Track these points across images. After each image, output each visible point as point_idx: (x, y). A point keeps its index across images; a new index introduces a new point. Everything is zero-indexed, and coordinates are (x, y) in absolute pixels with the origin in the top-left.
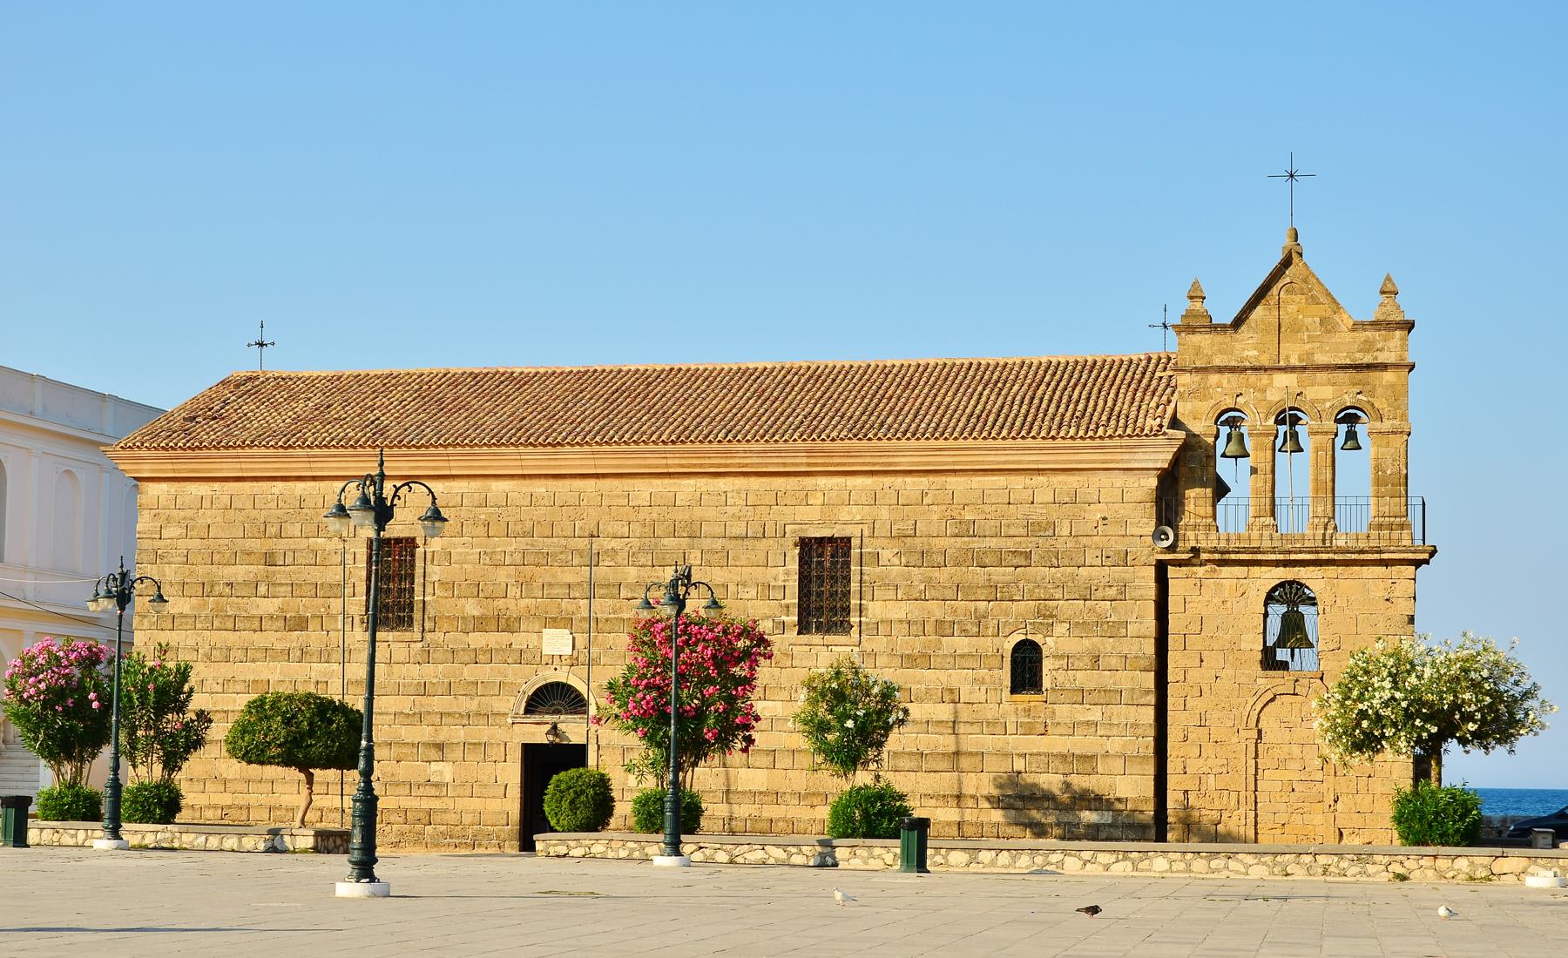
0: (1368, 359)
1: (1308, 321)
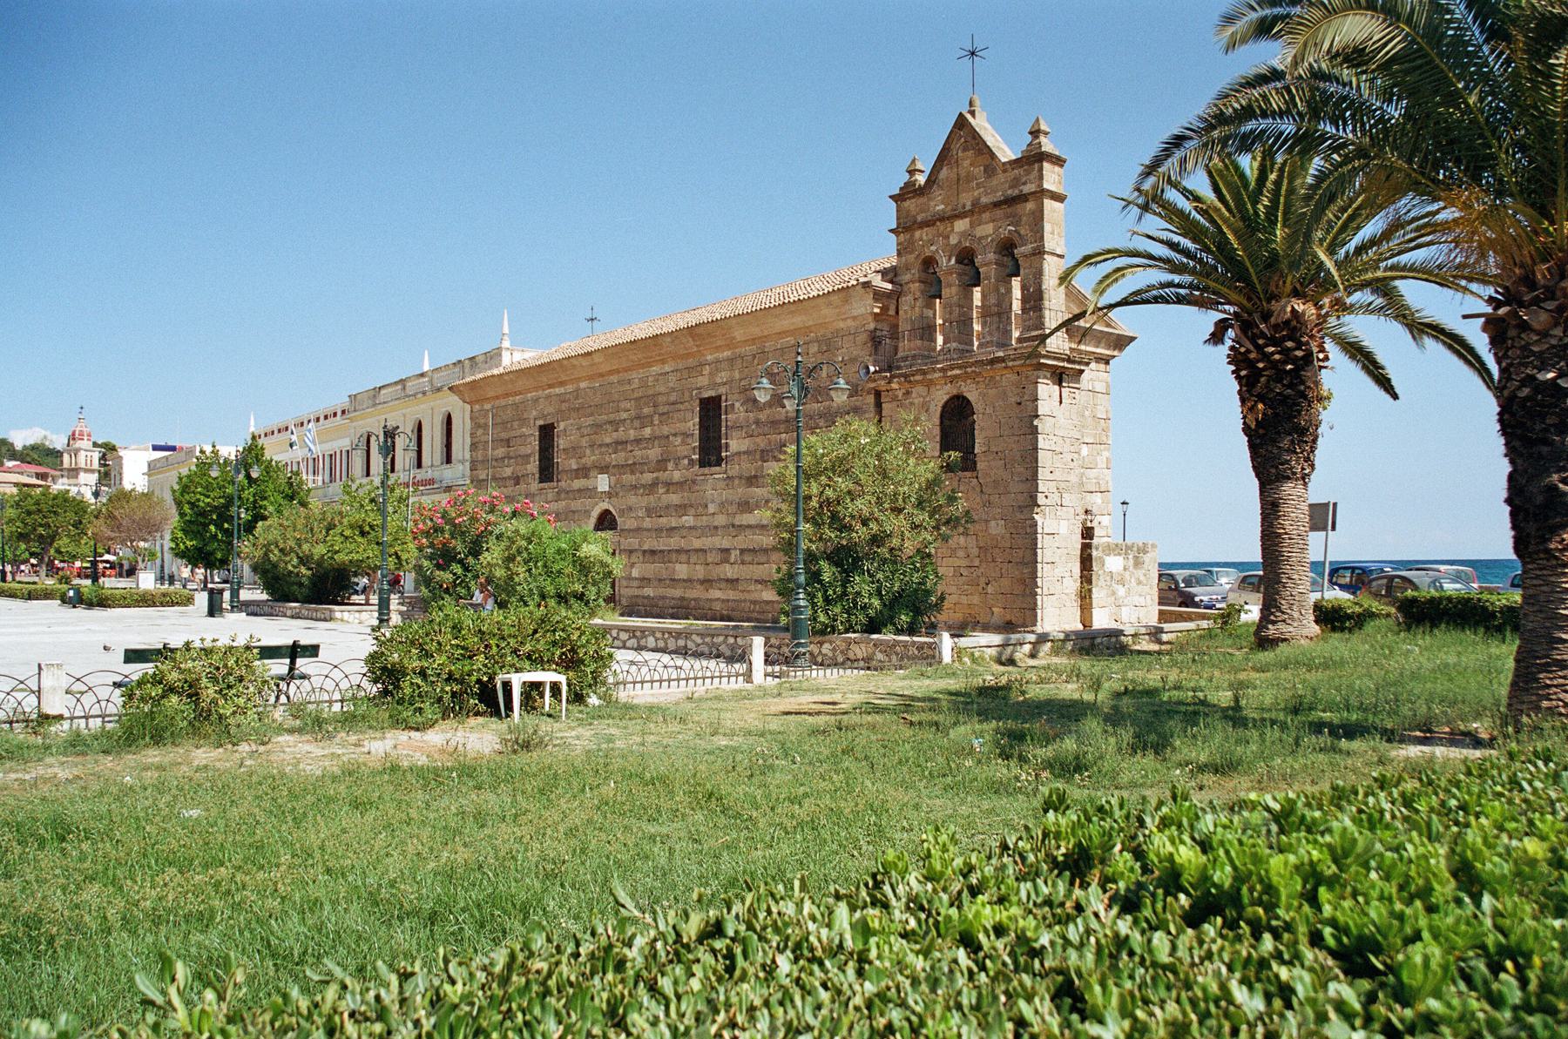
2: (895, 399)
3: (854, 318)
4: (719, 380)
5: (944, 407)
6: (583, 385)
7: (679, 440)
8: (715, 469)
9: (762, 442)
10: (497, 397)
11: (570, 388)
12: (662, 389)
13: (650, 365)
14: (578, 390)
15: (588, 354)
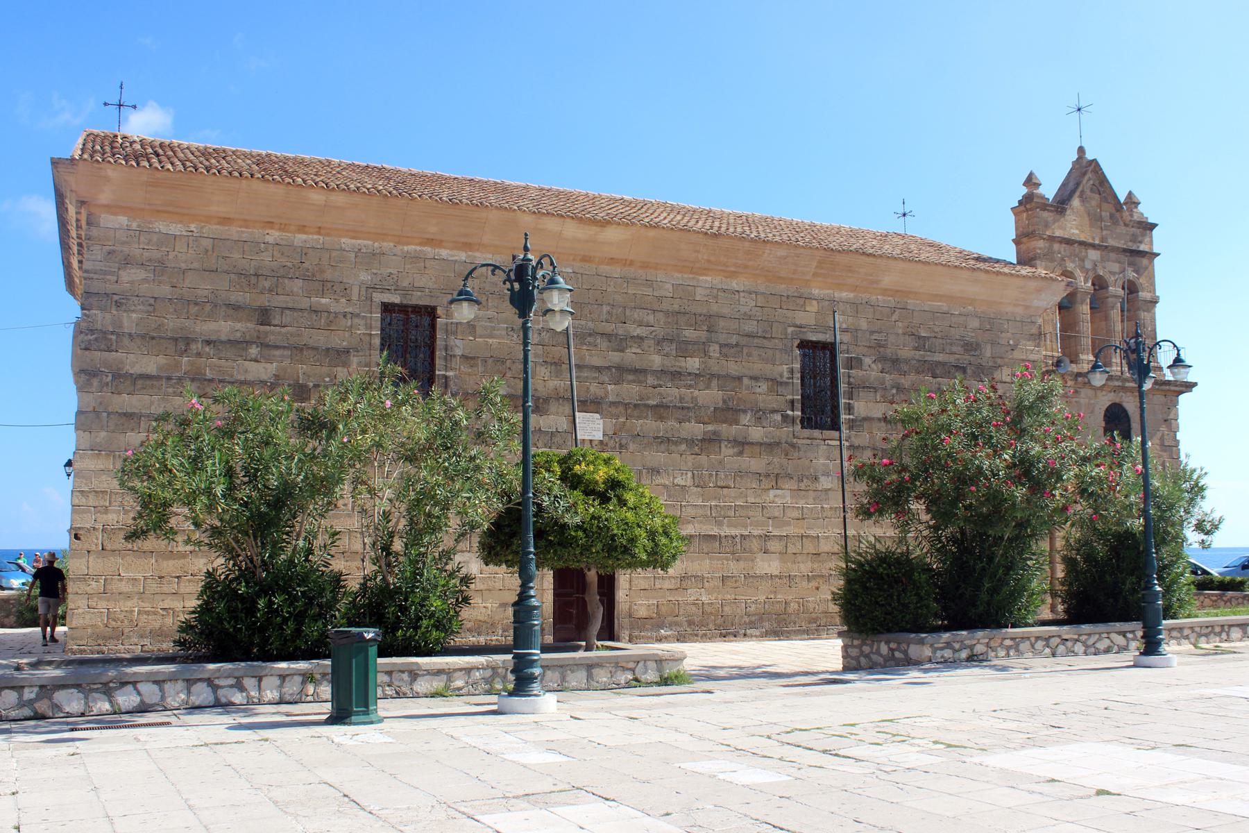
10: (225, 221)
12: (726, 311)
13: (705, 271)
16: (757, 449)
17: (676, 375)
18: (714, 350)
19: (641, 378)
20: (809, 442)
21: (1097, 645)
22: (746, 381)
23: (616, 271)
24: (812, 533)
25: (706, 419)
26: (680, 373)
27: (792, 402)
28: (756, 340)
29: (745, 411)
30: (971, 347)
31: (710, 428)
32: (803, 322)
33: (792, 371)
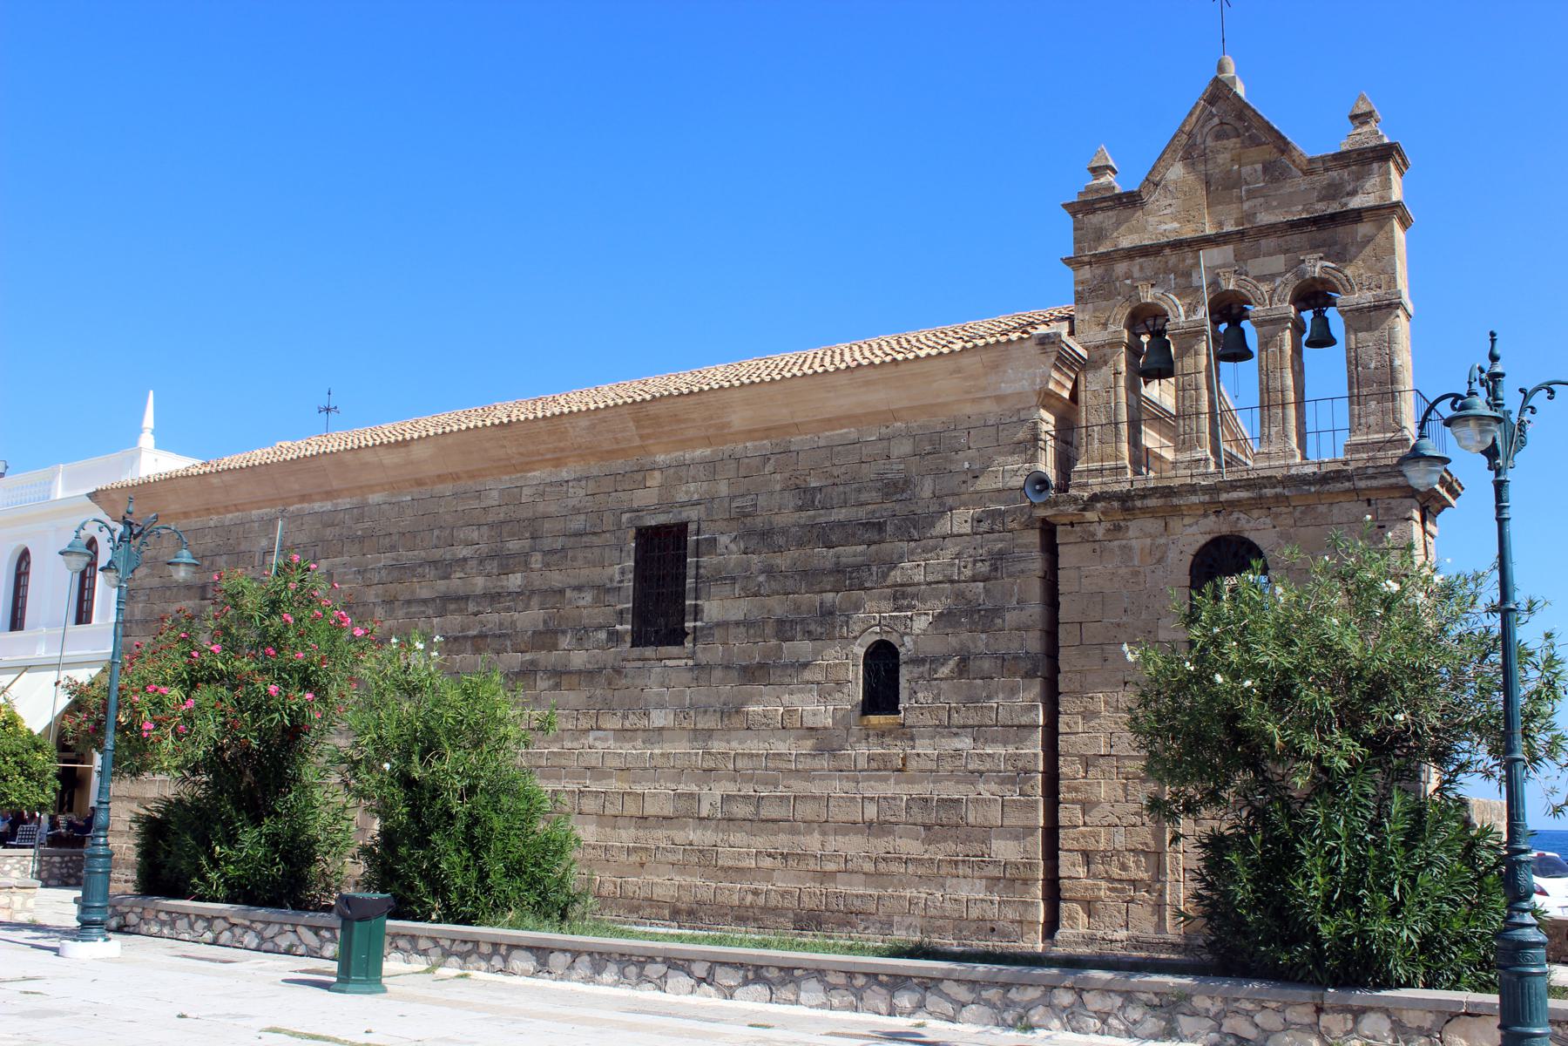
0: (1334, 207)
1: (1246, 170)
2: (1089, 538)
3: (999, 399)
4: (682, 497)
5: (1195, 556)
6: (375, 498)
7: (588, 597)
8: (674, 650)
9: (778, 606)
10: (186, 515)
11: (345, 502)
12: (553, 509)
13: (527, 466)
14: (362, 506)
15: (405, 443)
16: (575, 679)
17: (493, 597)
18: (536, 561)
19: (463, 605)
20: (640, 664)
21: (277, 940)
22: (568, 593)
23: (447, 488)
24: (638, 789)
25: (523, 647)
26: (499, 594)
27: (621, 612)
28: (585, 539)
29: (564, 632)
30: (895, 488)
31: (528, 656)
32: (642, 503)
33: (623, 573)
